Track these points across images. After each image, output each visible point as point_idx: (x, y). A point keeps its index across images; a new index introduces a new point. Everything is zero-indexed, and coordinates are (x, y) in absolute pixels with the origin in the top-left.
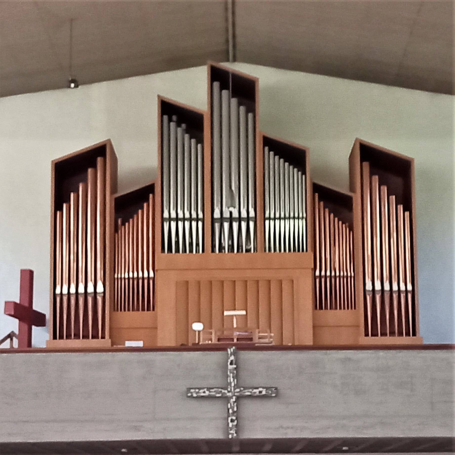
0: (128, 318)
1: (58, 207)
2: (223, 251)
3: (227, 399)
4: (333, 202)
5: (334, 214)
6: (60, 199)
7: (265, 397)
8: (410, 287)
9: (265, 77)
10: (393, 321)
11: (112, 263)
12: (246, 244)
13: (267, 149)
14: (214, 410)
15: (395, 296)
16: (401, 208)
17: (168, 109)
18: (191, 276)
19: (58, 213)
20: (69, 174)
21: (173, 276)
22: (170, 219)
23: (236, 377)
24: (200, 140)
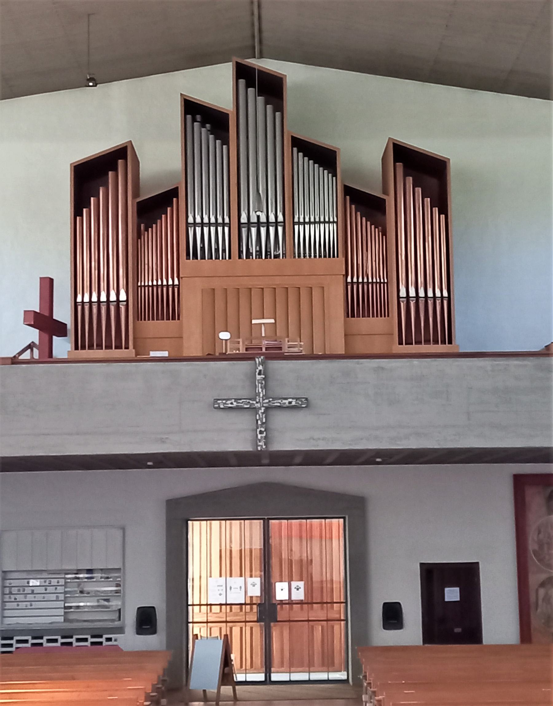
0: (154, 327)
1: (77, 212)
2: (251, 257)
4: (366, 205)
5: (54, 335)
6: (80, 204)
8: (445, 294)
9: (294, 74)
11: (135, 269)
12: (275, 250)
13: (295, 149)
15: (430, 302)
16: (436, 210)
17: (192, 109)
18: (216, 283)
19: (139, 240)
20: (90, 177)
21: (199, 283)
22: (249, 224)
24: (225, 142)
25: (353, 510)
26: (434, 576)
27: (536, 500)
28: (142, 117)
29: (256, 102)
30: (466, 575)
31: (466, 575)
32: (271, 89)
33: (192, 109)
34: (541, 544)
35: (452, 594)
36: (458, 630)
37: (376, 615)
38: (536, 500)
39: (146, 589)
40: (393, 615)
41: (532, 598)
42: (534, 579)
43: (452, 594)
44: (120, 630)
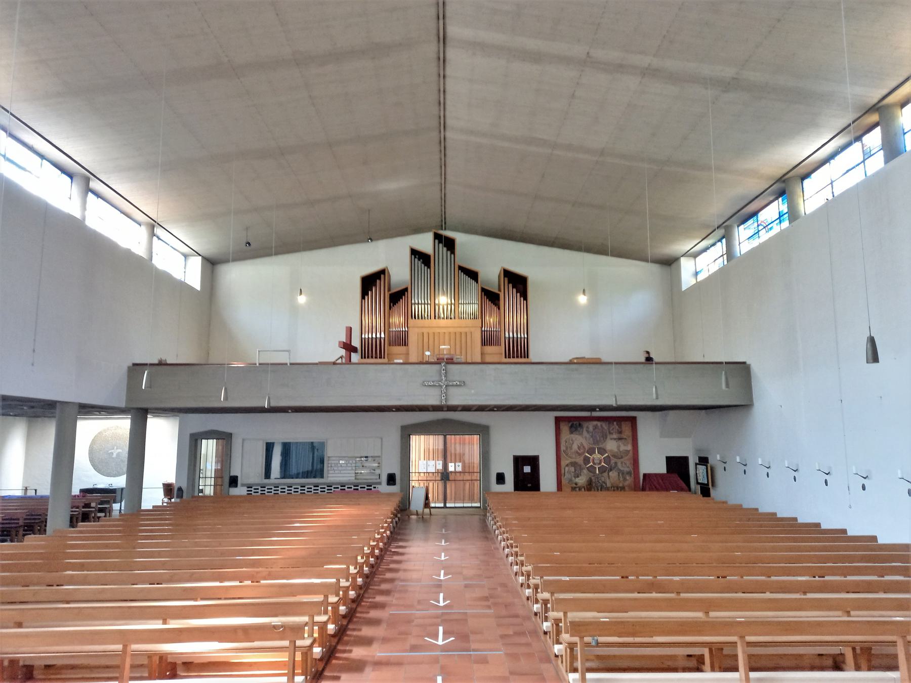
4: (491, 297)
6: (364, 294)
7: (457, 385)
9: (460, 238)
17: (414, 253)
20: (369, 283)
23: (446, 376)
25: (483, 431)
26: (519, 461)
27: (565, 428)
28: (392, 256)
29: (443, 250)
30: (534, 461)
31: (534, 461)
32: (450, 244)
37: (494, 478)
38: (565, 428)
40: (501, 478)
41: (563, 471)
43: (527, 469)
44: (380, 483)
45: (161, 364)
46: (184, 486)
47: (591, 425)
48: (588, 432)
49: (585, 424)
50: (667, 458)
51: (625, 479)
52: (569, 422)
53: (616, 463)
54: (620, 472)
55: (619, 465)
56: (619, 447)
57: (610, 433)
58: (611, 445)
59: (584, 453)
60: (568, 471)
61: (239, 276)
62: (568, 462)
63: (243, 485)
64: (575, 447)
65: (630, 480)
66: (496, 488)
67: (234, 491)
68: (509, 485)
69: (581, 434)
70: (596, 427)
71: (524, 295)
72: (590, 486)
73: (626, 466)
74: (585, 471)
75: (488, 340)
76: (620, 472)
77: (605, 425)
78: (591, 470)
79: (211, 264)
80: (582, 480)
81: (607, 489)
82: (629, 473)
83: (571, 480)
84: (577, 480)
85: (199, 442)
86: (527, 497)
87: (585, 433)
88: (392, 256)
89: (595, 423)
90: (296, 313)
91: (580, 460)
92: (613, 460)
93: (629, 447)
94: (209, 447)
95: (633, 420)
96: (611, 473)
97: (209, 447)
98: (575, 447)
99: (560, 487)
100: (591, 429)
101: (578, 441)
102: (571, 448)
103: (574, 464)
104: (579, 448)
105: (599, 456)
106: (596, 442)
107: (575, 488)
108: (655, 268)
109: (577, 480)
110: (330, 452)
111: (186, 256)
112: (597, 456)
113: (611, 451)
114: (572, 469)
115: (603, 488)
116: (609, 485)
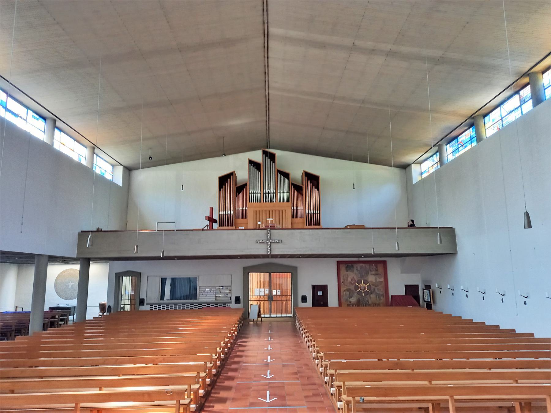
1: (220, 190)
3: (268, 243)
4: (297, 188)
6: (221, 187)
7: (277, 242)
9: (278, 153)
10: (314, 222)
14: (264, 246)
20: (224, 181)
23: (270, 237)
25: (294, 270)
26: (315, 288)
27: (343, 268)
28: (238, 164)
29: (268, 160)
30: (324, 288)
31: (324, 288)
32: (272, 157)
33: (251, 162)
34: (344, 280)
35: (320, 293)
36: (322, 303)
38: (343, 268)
39: (237, 292)
40: (304, 299)
42: (342, 289)
43: (320, 293)
44: (231, 303)
45: (99, 231)
46: (112, 305)
47: (359, 266)
48: (357, 270)
49: (355, 265)
50: (405, 286)
51: (380, 299)
52: (346, 264)
53: (374, 289)
54: (377, 295)
55: (376, 290)
56: (376, 279)
57: (371, 271)
58: (371, 278)
59: (354, 283)
60: (345, 294)
61: (143, 177)
62: (345, 289)
63: (147, 304)
64: (349, 279)
65: (383, 299)
66: (301, 305)
67: (142, 308)
68: (309, 303)
69: (353, 271)
70: (361, 267)
71: (317, 187)
72: (359, 304)
73: (381, 292)
74: (356, 294)
75: (295, 215)
76: (377, 295)
77: (367, 266)
78: (360, 293)
79: (128, 170)
80: (353, 300)
81: (369, 305)
82: (383, 295)
83: (347, 300)
84: (351, 300)
85: (121, 278)
86: (321, 310)
87: (355, 271)
88: (238, 164)
89: (362, 264)
90: (179, 199)
91: (352, 288)
92: (373, 287)
93: (382, 280)
94: (127, 281)
95: (384, 262)
96: (371, 296)
97: (127, 281)
98: (349, 279)
99: (340, 304)
100: (359, 268)
101: (351, 276)
102: (347, 280)
103: (349, 290)
104: (352, 280)
105: (364, 285)
106: (362, 276)
107: (350, 305)
108: (396, 170)
109: (351, 300)
110: (200, 284)
111: (113, 166)
112: (363, 285)
113: (371, 282)
114: (348, 293)
115: (367, 304)
116: (370, 303)
